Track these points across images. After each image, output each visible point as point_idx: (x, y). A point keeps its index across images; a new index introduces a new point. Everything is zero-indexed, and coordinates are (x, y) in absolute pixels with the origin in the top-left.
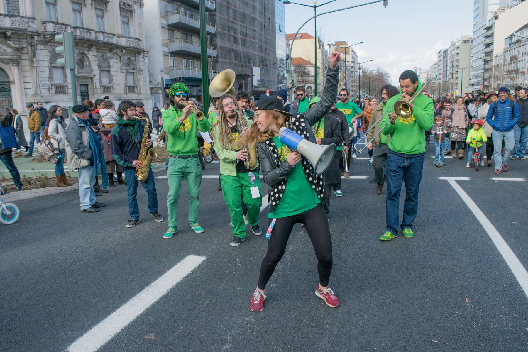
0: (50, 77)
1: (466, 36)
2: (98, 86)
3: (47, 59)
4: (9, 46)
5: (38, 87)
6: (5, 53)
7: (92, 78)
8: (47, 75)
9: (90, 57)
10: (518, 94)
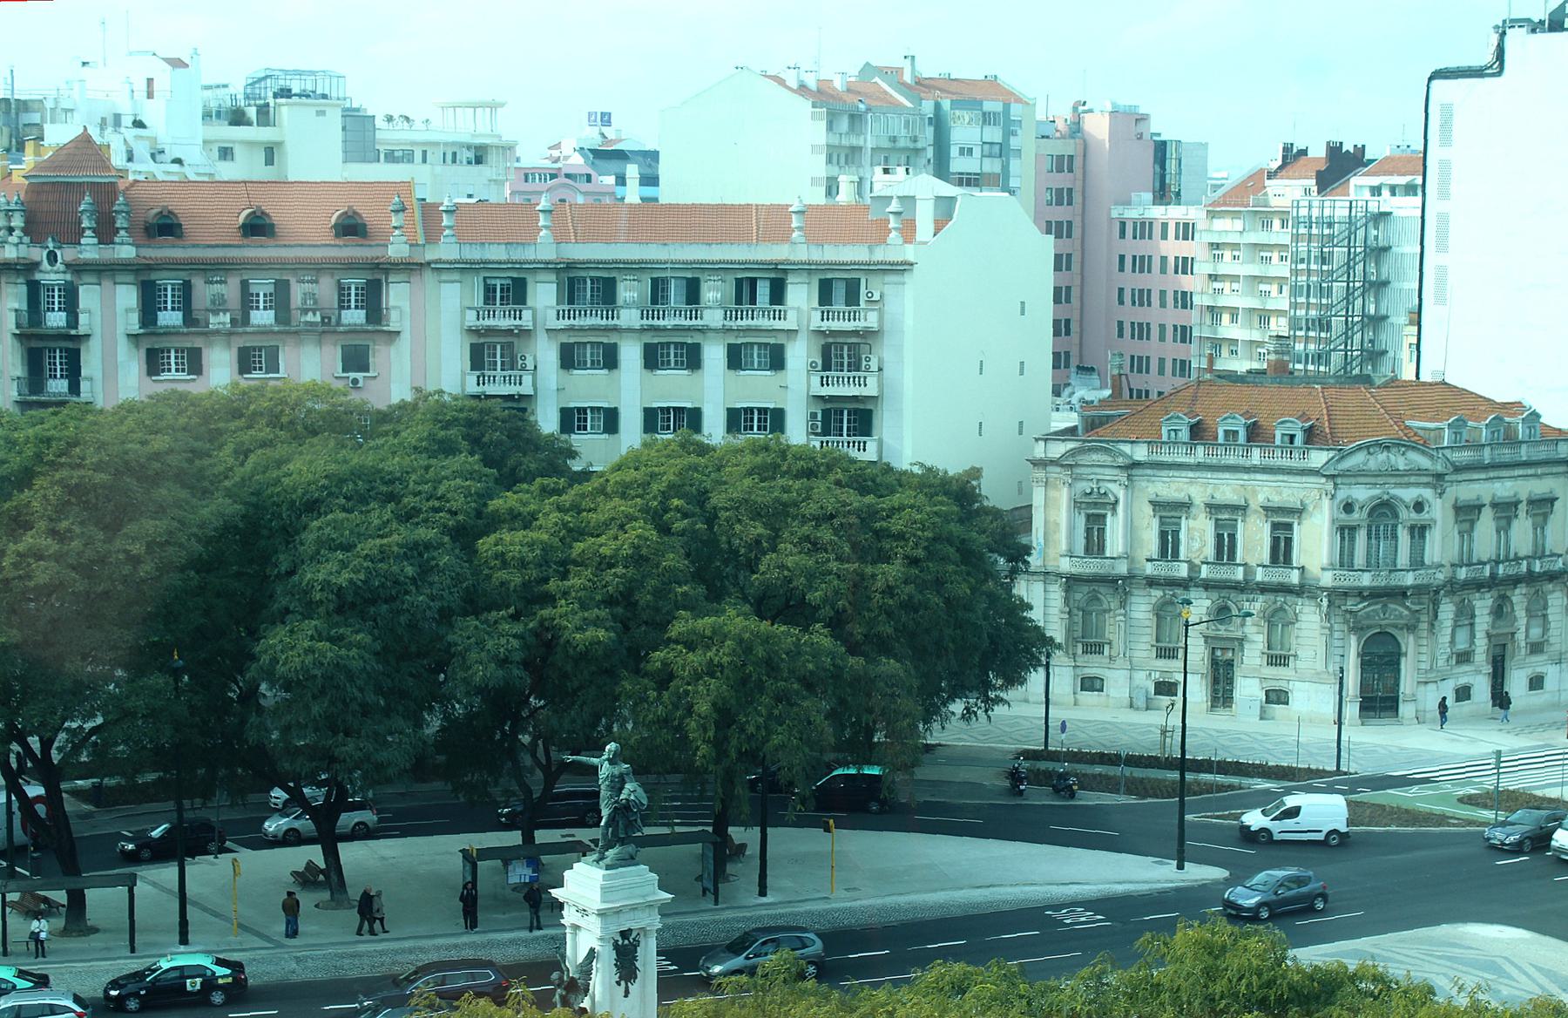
0: (1453, 642)
1: (1224, 747)
2: (1523, 644)
3: (1451, 616)
4: (1407, 608)
5: (1434, 659)
6: (1401, 616)
7: (1513, 634)
8: (1448, 639)
9: (1514, 599)
10: (1167, 986)
